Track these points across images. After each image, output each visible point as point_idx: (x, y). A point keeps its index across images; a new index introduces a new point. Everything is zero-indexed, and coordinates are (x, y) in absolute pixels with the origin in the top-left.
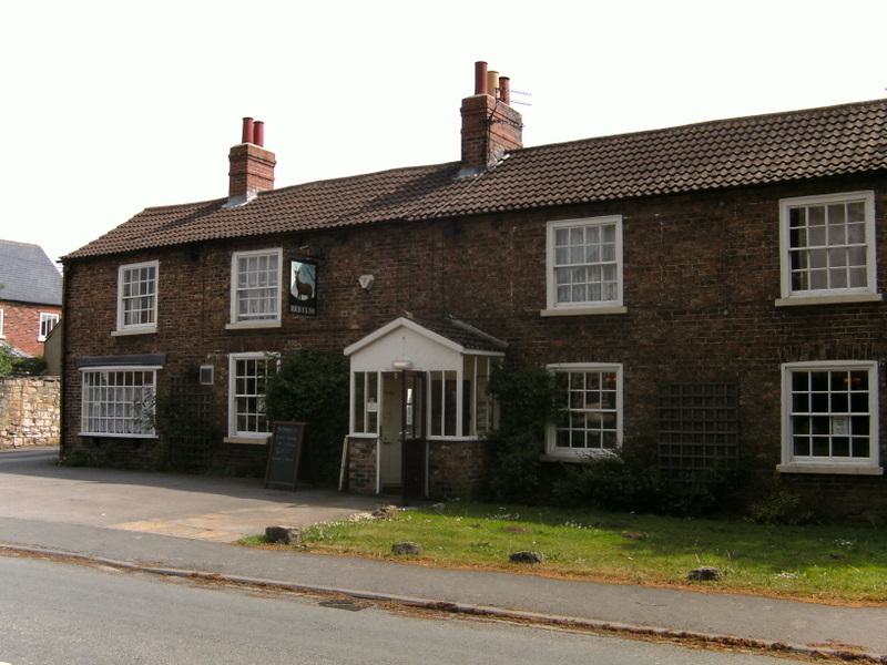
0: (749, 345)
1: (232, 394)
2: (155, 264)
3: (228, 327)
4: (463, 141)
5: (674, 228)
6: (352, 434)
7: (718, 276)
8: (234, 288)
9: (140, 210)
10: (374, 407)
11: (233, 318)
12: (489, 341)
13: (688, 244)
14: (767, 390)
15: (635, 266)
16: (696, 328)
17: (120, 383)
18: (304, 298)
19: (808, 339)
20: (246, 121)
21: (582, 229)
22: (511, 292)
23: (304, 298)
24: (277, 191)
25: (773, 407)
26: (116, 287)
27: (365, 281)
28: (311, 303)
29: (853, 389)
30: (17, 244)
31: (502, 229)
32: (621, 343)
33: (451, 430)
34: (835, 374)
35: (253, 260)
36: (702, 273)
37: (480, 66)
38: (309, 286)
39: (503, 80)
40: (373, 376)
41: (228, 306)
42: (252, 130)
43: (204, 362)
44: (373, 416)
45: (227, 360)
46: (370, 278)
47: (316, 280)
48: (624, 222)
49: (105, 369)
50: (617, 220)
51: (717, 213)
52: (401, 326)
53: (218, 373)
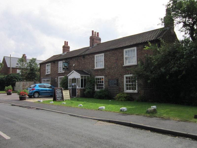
0: (120, 73)
1: (125, 83)
2: (50, 64)
3: (58, 73)
4: (90, 43)
5: (110, 55)
6: (68, 88)
7: (116, 62)
9: (53, 56)
11: (59, 71)
12: (88, 74)
13: (112, 57)
14: (122, 80)
15: (106, 61)
16: (113, 70)
17: (48, 81)
18: (66, 68)
19: (127, 71)
20: (65, 42)
21: (129, 50)
22: (91, 66)
23: (66, 68)
24: (102, 43)
25: (123, 82)
27: (74, 65)
28: (67, 69)
29: (99, 80)
31: (90, 56)
32: (104, 73)
34: (129, 77)
35: (98, 56)
36: (114, 62)
37: (93, 31)
38: (67, 66)
39: (98, 33)
41: (58, 69)
46: (74, 65)
47: (68, 65)
48: (104, 54)
49: (46, 80)
50: (103, 54)
51: (116, 52)
52: (73, 72)
53: (57, 80)
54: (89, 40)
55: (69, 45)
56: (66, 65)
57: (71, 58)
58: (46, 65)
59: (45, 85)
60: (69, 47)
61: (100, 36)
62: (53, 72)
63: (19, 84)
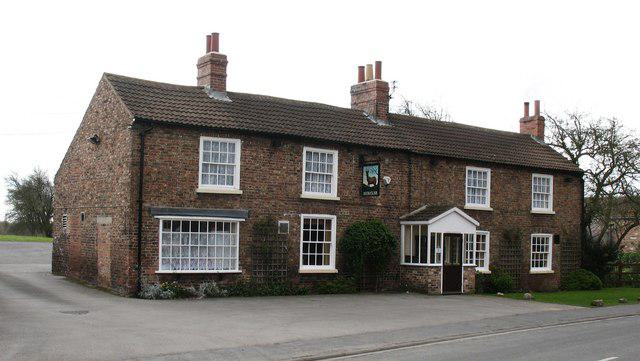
8: (201, 162)
10: (439, 250)
18: (372, 185)
23: (372, 185)
26: (198, 153)
30: (484, 129)
33: (424, 260)
40: (439, 235)
42: (213, 41)
43: (281, 218)
44: (439, 255)
45: (299, 218)
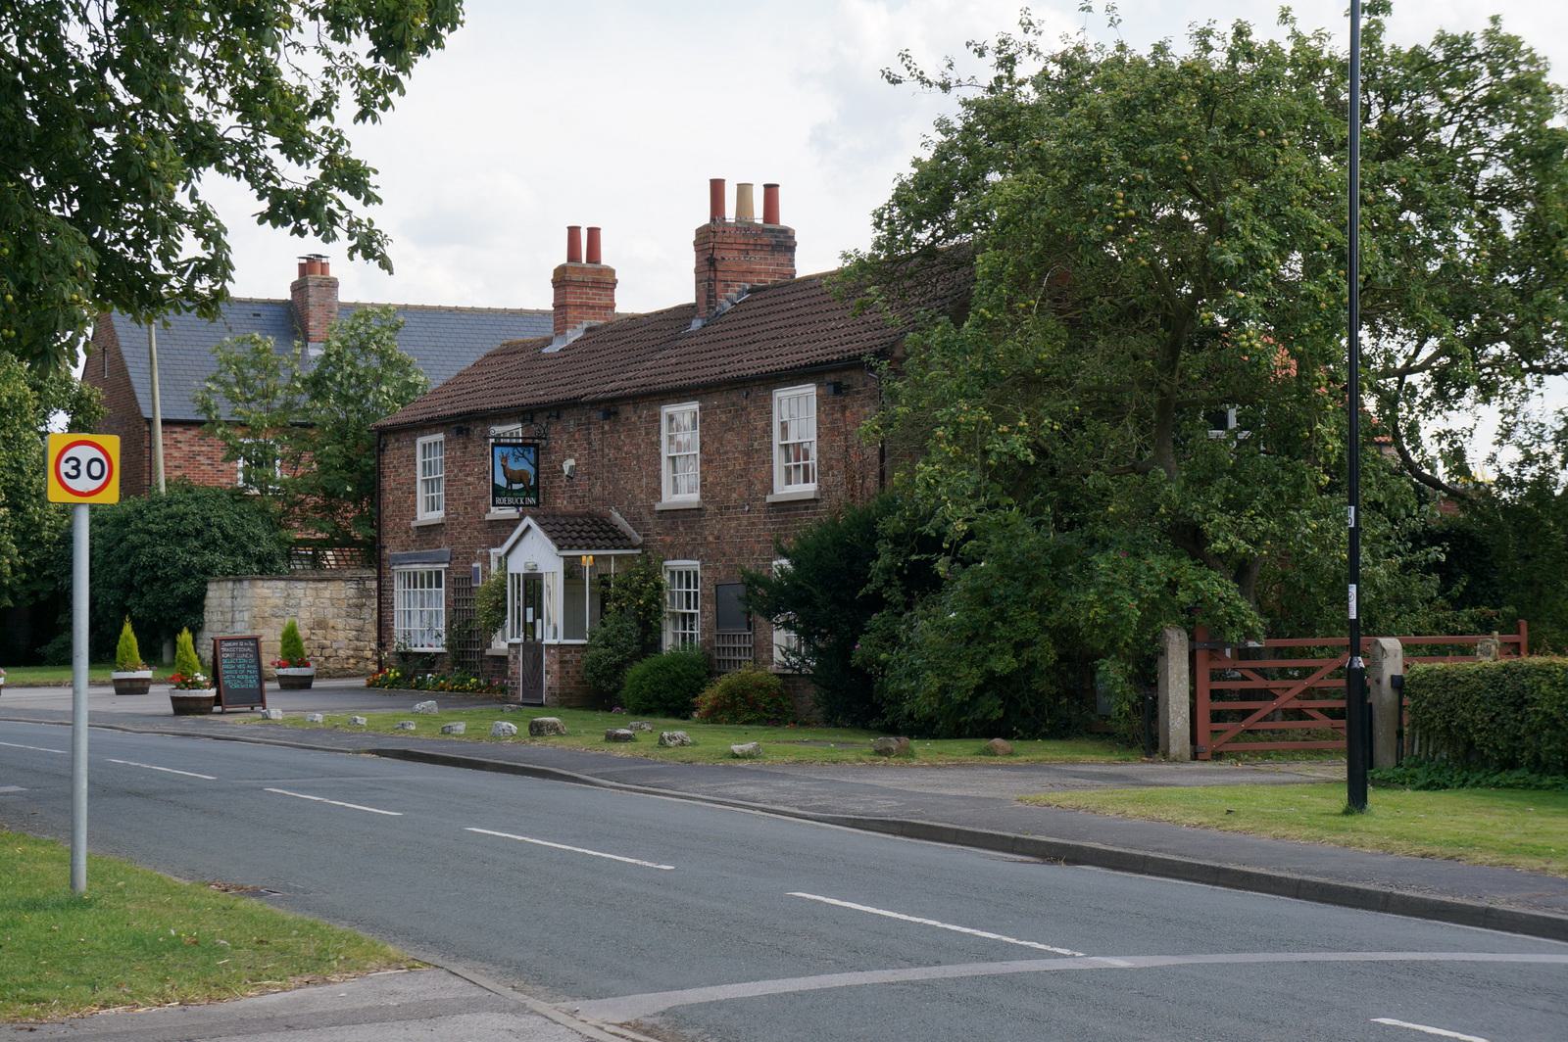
2: (440, 437)
16: (734, 524)
20: (573, 232)
47: (536, 466)
52: (528, 528)
54: (693, 254)
55: (606, 259)
56: (515, 466)
57: (557, 409)
58: (420, 441)
59: (121, 646)
60: (612, 272)
61: (788, 217)
62: (461, 510)
63: (229, 602)
